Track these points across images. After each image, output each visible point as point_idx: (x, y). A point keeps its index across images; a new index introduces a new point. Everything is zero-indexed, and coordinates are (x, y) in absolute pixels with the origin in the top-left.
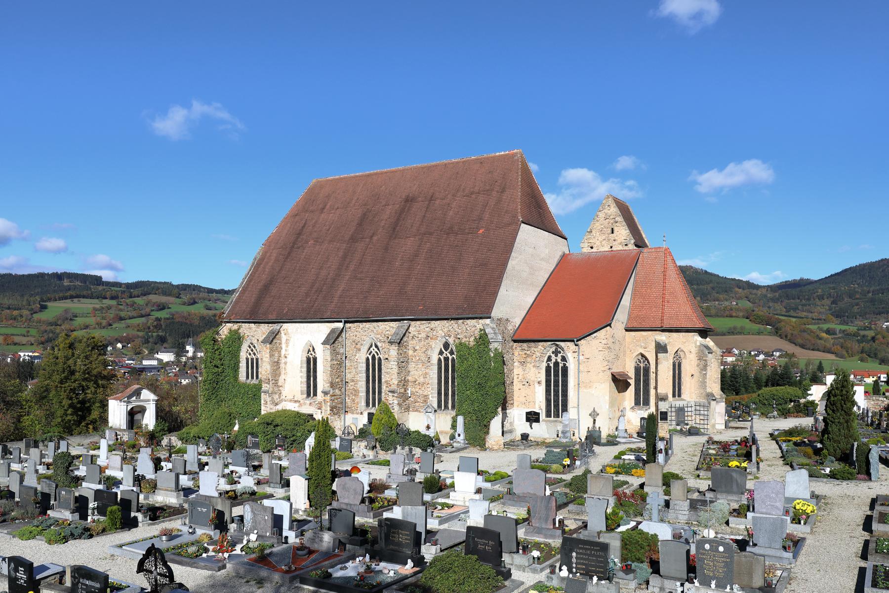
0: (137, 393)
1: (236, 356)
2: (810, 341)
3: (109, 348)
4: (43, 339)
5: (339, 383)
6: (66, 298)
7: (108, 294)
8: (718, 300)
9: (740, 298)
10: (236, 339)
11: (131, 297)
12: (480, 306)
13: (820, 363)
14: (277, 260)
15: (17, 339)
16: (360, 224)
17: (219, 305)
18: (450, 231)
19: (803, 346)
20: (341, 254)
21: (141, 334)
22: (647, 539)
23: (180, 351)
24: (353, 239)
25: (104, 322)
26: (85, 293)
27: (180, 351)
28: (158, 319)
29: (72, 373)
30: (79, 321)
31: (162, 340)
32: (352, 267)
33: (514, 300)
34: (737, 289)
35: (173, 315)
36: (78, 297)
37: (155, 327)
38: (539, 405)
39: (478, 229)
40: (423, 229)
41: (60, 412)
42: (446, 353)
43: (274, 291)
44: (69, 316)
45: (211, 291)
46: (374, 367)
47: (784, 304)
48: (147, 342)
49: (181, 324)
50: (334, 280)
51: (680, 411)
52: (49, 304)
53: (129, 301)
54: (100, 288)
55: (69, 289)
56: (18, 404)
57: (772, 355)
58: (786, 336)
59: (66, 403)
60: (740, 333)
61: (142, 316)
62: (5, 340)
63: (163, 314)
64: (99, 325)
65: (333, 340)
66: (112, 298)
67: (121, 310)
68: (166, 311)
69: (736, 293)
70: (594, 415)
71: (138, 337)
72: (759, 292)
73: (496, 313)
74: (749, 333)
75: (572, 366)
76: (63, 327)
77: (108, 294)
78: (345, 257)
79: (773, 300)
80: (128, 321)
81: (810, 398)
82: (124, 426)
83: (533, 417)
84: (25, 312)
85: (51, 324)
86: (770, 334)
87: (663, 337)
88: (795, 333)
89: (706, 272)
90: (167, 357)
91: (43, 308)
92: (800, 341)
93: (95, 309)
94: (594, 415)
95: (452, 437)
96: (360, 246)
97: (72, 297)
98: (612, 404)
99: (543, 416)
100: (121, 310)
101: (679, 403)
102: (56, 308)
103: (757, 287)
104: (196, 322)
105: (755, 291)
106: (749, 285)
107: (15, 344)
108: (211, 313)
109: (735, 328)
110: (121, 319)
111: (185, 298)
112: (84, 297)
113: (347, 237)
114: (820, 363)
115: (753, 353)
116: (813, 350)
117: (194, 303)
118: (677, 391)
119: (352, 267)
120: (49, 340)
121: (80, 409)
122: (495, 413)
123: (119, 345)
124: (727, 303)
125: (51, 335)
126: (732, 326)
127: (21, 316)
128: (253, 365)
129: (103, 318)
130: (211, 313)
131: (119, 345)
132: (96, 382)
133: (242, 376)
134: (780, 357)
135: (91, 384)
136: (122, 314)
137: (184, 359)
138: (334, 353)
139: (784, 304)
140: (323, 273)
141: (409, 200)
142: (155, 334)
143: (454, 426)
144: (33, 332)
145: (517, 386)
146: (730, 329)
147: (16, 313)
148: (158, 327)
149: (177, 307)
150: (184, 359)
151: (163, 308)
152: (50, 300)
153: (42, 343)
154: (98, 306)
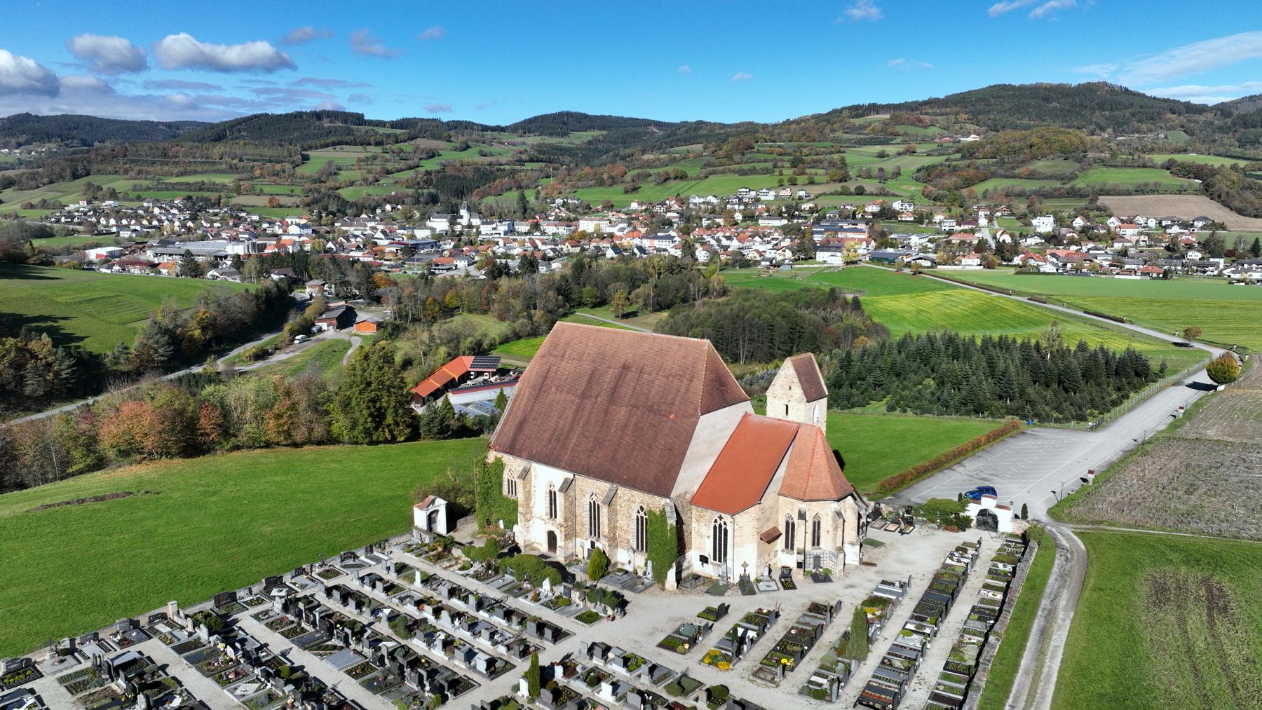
0: (433, 502)
1: (500, 477)
2: (1251, 203)
3: (378, 211)
4: (308, 200)
5: (571, 516)
6: (327, 146)
7: (372, 140)
8: (1138, 132)
9: (1172, 128)
10: (500, 465)
11: (397, 142)
12: (662, 487)
13: (1257, 240)
14: (529, 400)
15: (283, 200)
16: (589, 382)
17: (496, 148)
18: (651, 409)
19: (1241, 212)
20: (574, 407)
21: (410, 191)
22: (1037, 415)
23: (453, 214)
24: (584, 396)
25: (370, 177)
26: (347, 139)
27: (453, 214)
28: (428, 173)
29: (369, 384)
30: (344, 176)
31: (434, 200)
32: (581, 424)
33: (691, 477)
34: (1169, 115)
35: (445, 166)
36: (340, 143)
37: (426, 182)
38: (709, 552)
39: (670, 413)
40: (633, 402)
41: (361, 421)
42: (642, 514)
43: (526, 431)
44: (333, 170)
45: (485, 128)
46: (594, 510)
47: (1238, 135)
48: (417, 202)
49: (454, 178)
50: (568, 432)
51: (817, 558)
52: (311, 153)
53: (395, 147)
54: (363, 129)
55: (329, 132)
56: (327, 413)
57: (1192, 225)
58: (1219, 196)
59: (365, 412)
60: (1153, 192)
61: (410, 168)
62: (270, 202)
63: (431, 165)
64: (366, 182)
65: (567, 486)
66: (378, 144)
67: (387, 161)
68: (436, 160)
69: (1168, 120)
70: (745, 565)
71: (408, 196)
72: (1202, 118)
73: (673, 495)
74: (1166, 192)
75: (729, 528)
76: (327, 184)
77: (372, 140)
78: (577, 411)
79: (1222, 130)
80: (396, 175)
81: (967, 514)
82: (425, 528)
83: (704, 559)
84: (288, 166)
85: (315, 181)
86: (1197, 192)
87: (803, 506)
88: (1232, 192)
89: (1126, 90)
90: (441, 224)
91: (306, 158)
92: (1237, 204)
93: (360, 160)
94: (745, 565)
95: (645, 573)
96: (588, 403)
97: (334, 144)
98: (760, 555)
99: (711, 559)
100: (387, 161)
101: (816, 552)
102: (320, 158)
103: (1202, 109)
104: (470, 174)
105: (1196, 117)
106: (1190, 108)
107: (281, 206)
108: (486, 160)
109: (1146, 185)
110: (389, 172)
111: (459, 140)
112: (347, 143)
113: (579, 392)
114: (1257, 240)
115: (1164, 223)
116: (1256, 216)
117: (468, 147)
118: (816, 541)
119: (581, 424)
120: (315, 202)
121: (377, 416)
122: (671, 567)
123: (388, 207)
124: (1151, 136)
125: (316, 195)
126: (1142, 181)
127: (284, 171)
128: (512, 485)
129: (370, 172)
130: (486, 160)
131: (388, 207)
132: (389, 391)
133: (505, 492)
134: (1202, 228)
135: (384, 393)
136: (390, 166)
137: (458, 228)
138: (566, 497)
139: (1238, 135)
140: (562, 423)
141: (625, 367)
142: (425, 191)
143: (646, 565)
144: (298, 190)
145: (694, 535)
146: (1139, 185)
147: (278, 167)
148: (428, 182)
149: (449, 155)
150: (458, 228)
151: (433, 156)
152: (311, 148)
153: (308, 205)
154: (362, 155)
